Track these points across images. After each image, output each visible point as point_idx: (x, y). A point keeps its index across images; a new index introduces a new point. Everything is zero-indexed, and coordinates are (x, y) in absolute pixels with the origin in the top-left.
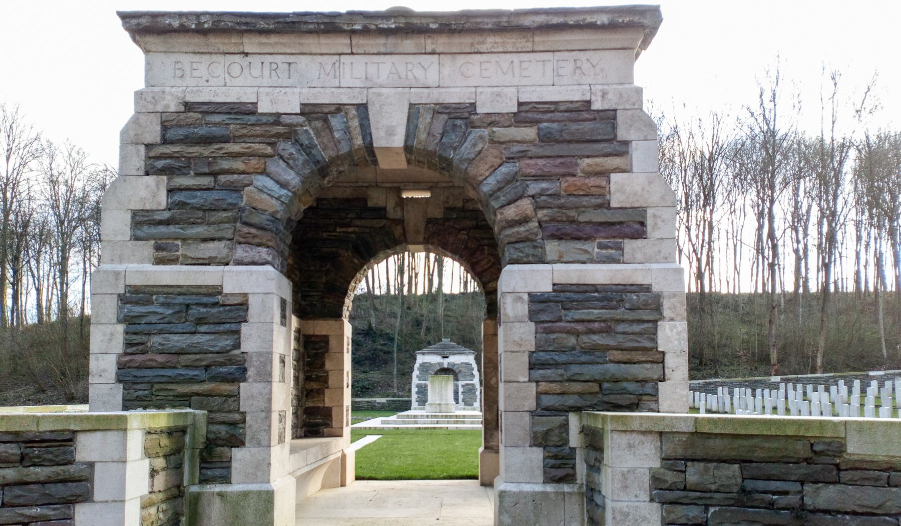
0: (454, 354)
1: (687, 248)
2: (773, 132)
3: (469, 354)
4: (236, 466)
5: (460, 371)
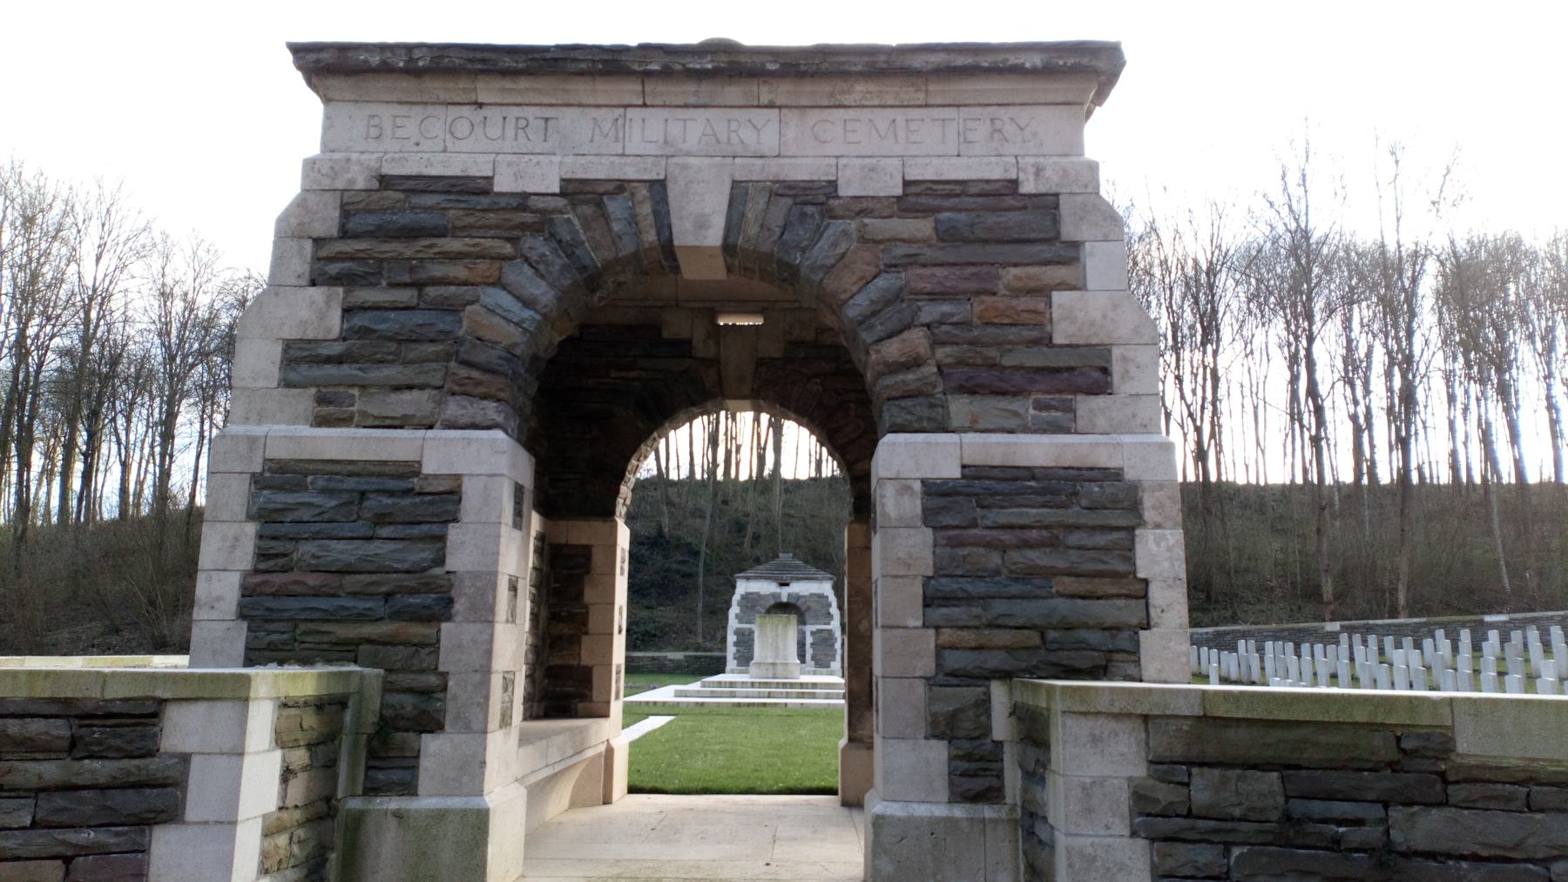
0: (798, 579)
5: (809, 608)
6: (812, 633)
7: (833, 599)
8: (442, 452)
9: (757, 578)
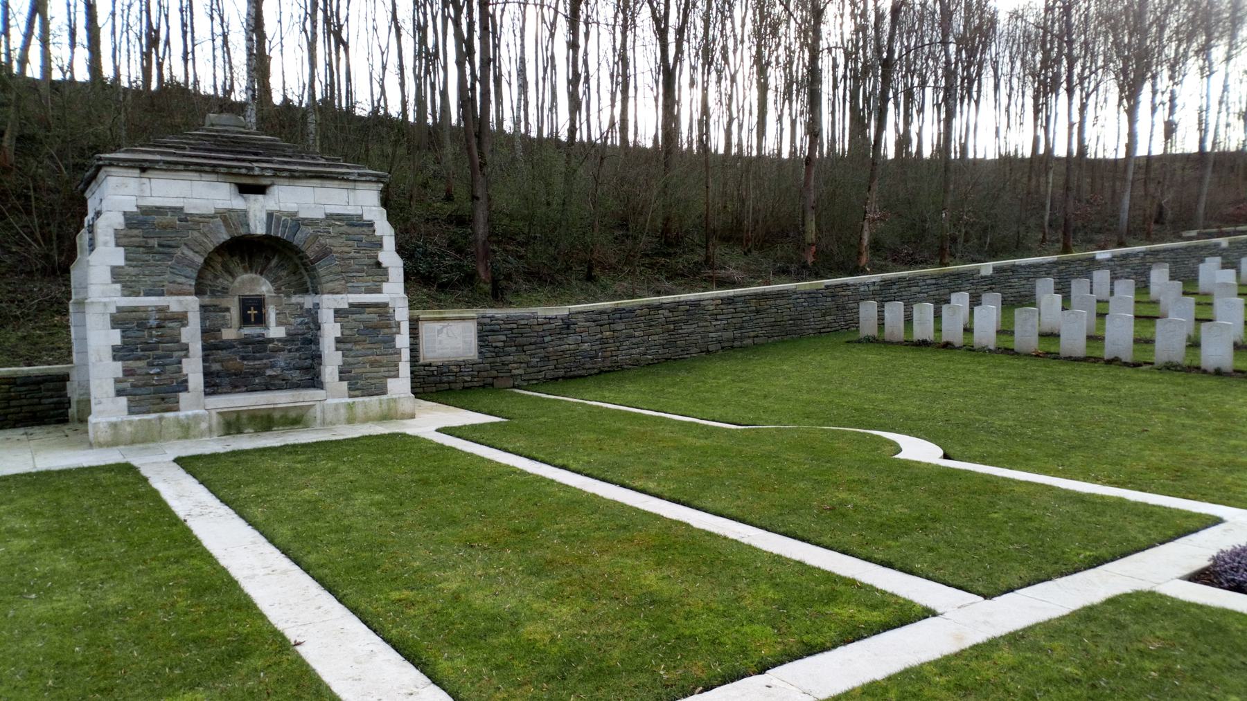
0: (293, 176)
1: (793, 24)
2: (366, 328)
3: (361, 179)
4: (182, 404)
5: (325, 253)
6: (339, 313)
7: (385, 230)
8: (174, 304)
9: (171, 167)
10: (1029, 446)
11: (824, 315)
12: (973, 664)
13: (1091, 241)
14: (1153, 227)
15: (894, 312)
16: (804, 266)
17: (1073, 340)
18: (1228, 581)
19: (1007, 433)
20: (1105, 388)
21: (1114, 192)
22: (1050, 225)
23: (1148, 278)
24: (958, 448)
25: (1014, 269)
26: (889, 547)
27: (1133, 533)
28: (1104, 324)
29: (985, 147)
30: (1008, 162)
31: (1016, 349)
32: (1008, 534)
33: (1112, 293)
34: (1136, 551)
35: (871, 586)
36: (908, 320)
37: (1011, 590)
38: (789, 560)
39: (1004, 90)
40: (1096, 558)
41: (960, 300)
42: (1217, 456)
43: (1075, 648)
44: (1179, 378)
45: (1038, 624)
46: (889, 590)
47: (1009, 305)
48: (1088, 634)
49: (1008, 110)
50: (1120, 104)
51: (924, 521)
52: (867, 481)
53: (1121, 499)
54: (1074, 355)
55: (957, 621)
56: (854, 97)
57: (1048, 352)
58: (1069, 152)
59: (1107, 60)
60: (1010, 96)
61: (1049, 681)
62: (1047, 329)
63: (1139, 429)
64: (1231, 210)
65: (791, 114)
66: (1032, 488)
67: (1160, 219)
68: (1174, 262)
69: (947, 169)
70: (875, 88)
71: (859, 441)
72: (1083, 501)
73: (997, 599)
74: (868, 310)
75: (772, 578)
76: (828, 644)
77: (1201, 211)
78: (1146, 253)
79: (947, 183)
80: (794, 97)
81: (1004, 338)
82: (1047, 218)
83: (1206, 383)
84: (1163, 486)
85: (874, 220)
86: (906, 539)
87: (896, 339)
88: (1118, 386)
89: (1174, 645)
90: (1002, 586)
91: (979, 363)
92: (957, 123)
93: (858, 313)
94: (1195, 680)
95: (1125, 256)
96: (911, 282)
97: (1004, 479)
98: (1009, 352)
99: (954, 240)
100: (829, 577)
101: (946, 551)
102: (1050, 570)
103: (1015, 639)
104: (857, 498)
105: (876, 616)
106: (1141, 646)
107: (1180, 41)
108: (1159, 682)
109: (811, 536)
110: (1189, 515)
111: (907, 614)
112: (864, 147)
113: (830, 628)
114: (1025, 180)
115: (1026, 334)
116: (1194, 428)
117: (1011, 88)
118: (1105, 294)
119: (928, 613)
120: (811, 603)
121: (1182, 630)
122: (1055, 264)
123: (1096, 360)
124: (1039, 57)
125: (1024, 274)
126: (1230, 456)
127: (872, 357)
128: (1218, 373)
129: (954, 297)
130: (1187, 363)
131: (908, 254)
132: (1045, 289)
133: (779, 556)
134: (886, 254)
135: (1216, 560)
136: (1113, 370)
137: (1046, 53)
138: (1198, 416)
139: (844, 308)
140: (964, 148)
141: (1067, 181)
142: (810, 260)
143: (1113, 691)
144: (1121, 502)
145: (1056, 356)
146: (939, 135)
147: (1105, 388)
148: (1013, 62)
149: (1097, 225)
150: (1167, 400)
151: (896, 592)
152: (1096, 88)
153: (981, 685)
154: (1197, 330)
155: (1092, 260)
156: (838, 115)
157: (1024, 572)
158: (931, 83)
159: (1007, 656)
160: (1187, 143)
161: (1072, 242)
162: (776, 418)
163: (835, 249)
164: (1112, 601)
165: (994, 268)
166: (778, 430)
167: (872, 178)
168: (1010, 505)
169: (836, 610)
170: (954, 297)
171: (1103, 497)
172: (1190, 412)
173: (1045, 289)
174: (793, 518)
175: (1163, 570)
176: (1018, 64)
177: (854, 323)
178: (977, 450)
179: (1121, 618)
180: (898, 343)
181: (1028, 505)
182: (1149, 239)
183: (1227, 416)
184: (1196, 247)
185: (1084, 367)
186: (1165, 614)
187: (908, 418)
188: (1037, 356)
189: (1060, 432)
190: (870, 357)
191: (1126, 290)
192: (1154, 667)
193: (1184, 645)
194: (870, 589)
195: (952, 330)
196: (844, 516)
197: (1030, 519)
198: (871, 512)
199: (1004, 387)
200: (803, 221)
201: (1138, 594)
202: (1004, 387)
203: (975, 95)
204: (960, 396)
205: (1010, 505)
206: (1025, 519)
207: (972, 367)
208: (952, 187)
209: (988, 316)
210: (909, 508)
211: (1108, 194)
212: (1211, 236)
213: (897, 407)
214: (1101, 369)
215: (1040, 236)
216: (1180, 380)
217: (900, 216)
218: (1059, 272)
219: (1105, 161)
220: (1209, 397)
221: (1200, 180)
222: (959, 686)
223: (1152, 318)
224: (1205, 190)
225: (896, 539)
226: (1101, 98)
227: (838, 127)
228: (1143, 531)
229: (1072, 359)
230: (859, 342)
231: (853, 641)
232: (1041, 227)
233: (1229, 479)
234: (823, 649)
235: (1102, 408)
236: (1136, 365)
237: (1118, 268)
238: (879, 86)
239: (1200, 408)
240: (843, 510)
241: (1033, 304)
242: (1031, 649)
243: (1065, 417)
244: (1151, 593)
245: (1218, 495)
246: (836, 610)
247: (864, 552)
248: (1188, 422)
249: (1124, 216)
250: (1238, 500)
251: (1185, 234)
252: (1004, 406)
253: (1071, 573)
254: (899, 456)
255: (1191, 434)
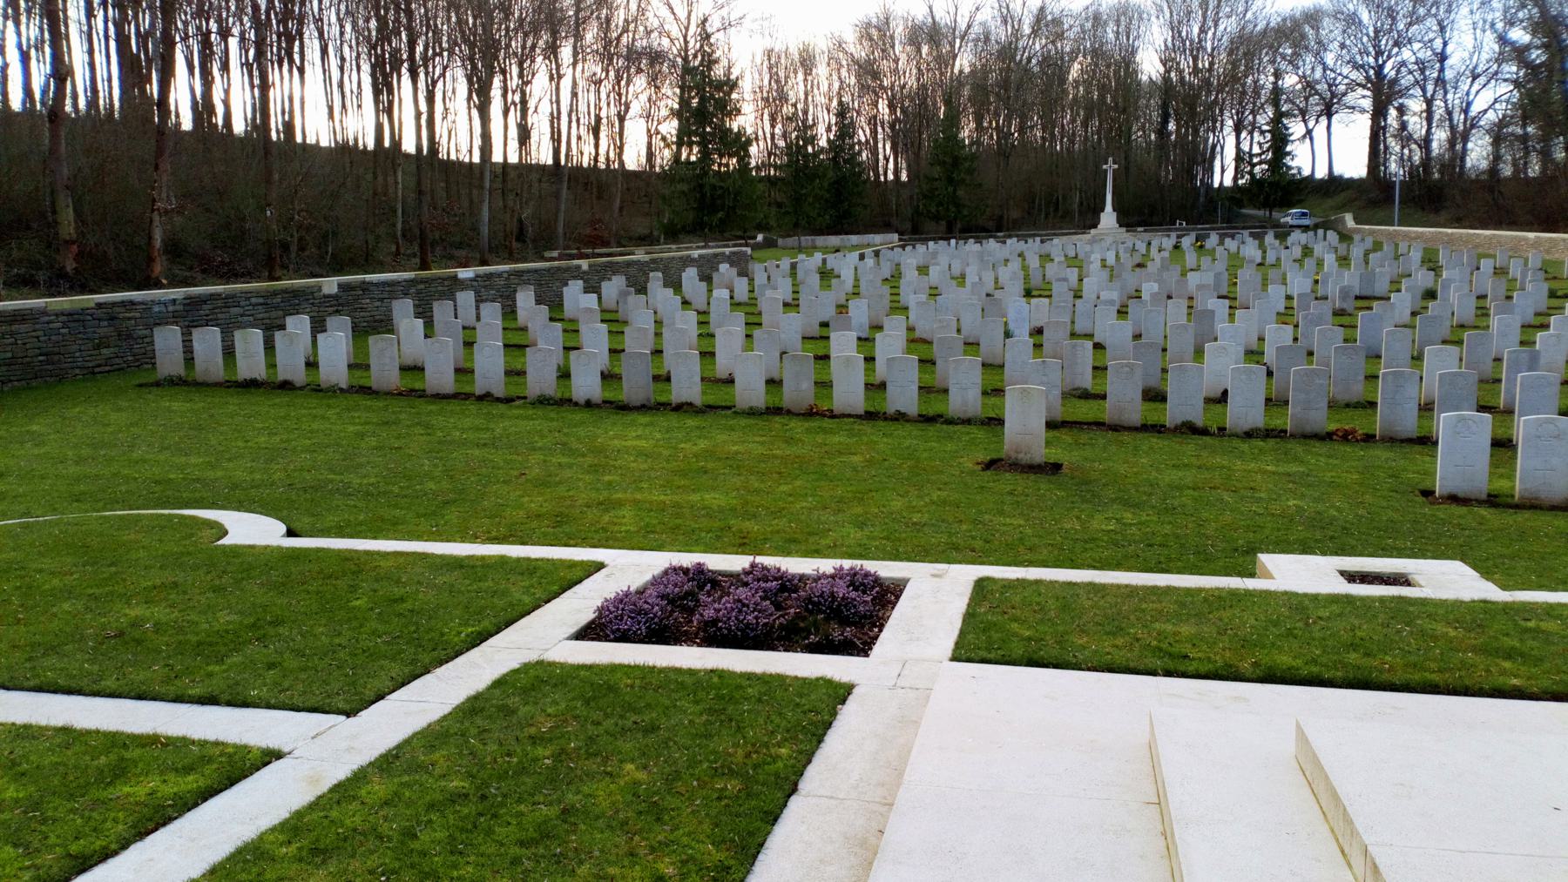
10: (396, 506)
11: (98, 347)
12: (334, 814)
13: (451, 257)
14: (515, 245)
15: (207, 341)
16: (62, 274)
17: (440, 376)
18: (613, 632)
19: (368, 494)
20: (478, 429)
21: (471, 202)
22: (404, 236)
23: (514, 301)
24: (306, 520)
25: (365, 287)
26: (210, 675)
27: (517, 595)
28: (472, 354)
29: (316, 129)
30: (346, 152)
31: (374, 387)
32: (374, 625)
33: (478, 319)
34: (523, 616)
35: (184, 739)
36: (229, 352)
37: (380, 697)
38: (47, 728)
39: (334, 62)
40: (480, 633)
41: (298, 325)
42: (594, 495)
43: (460, 754)
44: (552, 413)
45: (415, 735)
46: (211, 737)
47: (361, 332)
48: (474, 731)
49: (341, 85)
50: (470, 98)
51: (259, 628)
52: (175, 585)
53: (503, 557)
54: (443, 391)
55: (313, 754)
56: (123, 41)
57: (412, 389)
58: (419, 148)
59: (453, 43)
60: (342, 69)
61: (431, 807)
62: (409, 362)
63: (516, 473)
64: (588, 231)
65: (20, 46)
66: (401, 560)
67: (521, 236)
68: (538, 285)
69: (267, 153)
70: (152, 24)
71: (162, 528)
72: (462, 567)
73: (363, 713)
74: (167, 340)
75: (14, 764)
76: (113, 846)
77: (560, 230)
78: (511, 273)
79: (269, 173)
80: (23, 19)
81: (358, 373)
82: (399, 226)
83: (579, 416)
84: (545, 535)
85: (166, 212)
86: (236, 658)
87: (212, 378)
88: (492, 426)
89: (565, 721)
90: (369, 694)
91: (329, 406)
92: (275, 95)
93: (152, 343)
94: (589, 755)
95: (490, 276)
96: (229, 300)
97: (367, 553)
98: (366, 391)
99: (285, 247)
100: (115, 741)
101: (292, 662)
102: (427, 661)
103: (387, 763)
104: (160, 612)
105: (191, 782)
106: (533, 730)
107: (526, 35)
108: (554, 768)
109: (84, 683)
110: (572, 565)
111: (237, 766)
112: (143, 111)
113: (115, 820)
114: (369, 177)
115: (384, 368)
116: (570, 466)
117: (343, 59)
118: (471, 320)
119: (271, 756)
120: (84, 788)
121: (574, 699)
122: (412, 282)
123: (467, 396)
124: (373, 24)
125: (376, 293)
126: (605, 493)
127: (178, 406)
128: (589, 404)
129: (290, 321)
130: (559, 395)
131: (222, 263)
132: (403, 311)
133: (27, 727)
134: (188, 261)
135: (600, 610)
136: (486, 407)
137: (382, 22)
138: (573, 453)
139: (129, 336)
140: (289, 127)
141: (419, 183)
142: (70, 266)
143: (505, 796)
144: (503, 561)
145: (421, 394)
146: (254, 105)
147: (478, 429)
148: (342, 26)
149: (457, 239)
150: (542, 437)
151: (221, 739)
152: (443, 75)
153: (345, 839)
154: (567, 358)
155: (455, 278)
156: (99, 59)
157: (396, 670)
158: (236, 31)
159: (378, 788)
160: (542, 153)
161: (430, 257)
162: (22, 508)
163: (111, 251)
164: (499, 683)
165: (340, 285)
166: (26, 526)
167: (160, 152)
168: (376, 586)
169: (127, 789)
170: (290, 321)
171: (483, 558)
172: (566, 449)
173: (403, 311)
174: (52, 660)
175: (548, 635)
176: (348, 28)
177: (147, 358)
178: (331, 520)
179: (509, 702)
180: (218, 385)
181: (398, 582)
182: (511, 258)
183: (600, 451)
184: (559, 269)
185: (454, 406)
186: (556, 685)
187: (235, 487)
188: (400, 394)
189: (431, 485)
190: (176, 405)
191: (492, 313)
192: (547, 753)
193: (576, 717)
194: (183, 743)
195: (291, 365)
196: (139, 642)
197: (402, 600)
198: (181, 628)
199: (361, 436)
200: (53, 203)
201: (526, 668)
202: (362, 435)
203: (297, 57)
204: (307, 451)
205: (376, 586)
206: (395, 601)
207: (320, 412)
208: (276, 177)
209: (336, 345)
210: (240, 613)
211: (466, 204)
212: (572, 257)
213: (220, 474)
214: (472, 407)
215: (394, 248)
216: (553, 415)
217: (208, 210)
218: (419, 292)
219: (459, 164)
220: (581, 431)
221: (557, 195)
222: (315, 851)
223: (522, 347)
224: (563, 207)
225: (221, 661)
226: (449, 87)
227: (101, 72)
228: (526, 591)
229: (439, 397)
230: (157, 384)
231: (156, 829)
232: (395, 236)
233: (606, 518)
234: (106, 855)
235: (477, 452)
236: (508, 400)
237: (484, 289)
238: (159, 25)
239: (575, 445)
240: (137, 634)
241: (391, 331)
242: (407, 772)
243: (436, 466)
244: (540, 663)
245: (597, 537)
246: (127, 789)
247: (172, 690)
248: (564, 460)
249: (485, 230)
250: (617, 540)
251: (547, 254)
252: (364, 460)
253: (452, 659)
254: (225, 541)
255: (568, 473)
